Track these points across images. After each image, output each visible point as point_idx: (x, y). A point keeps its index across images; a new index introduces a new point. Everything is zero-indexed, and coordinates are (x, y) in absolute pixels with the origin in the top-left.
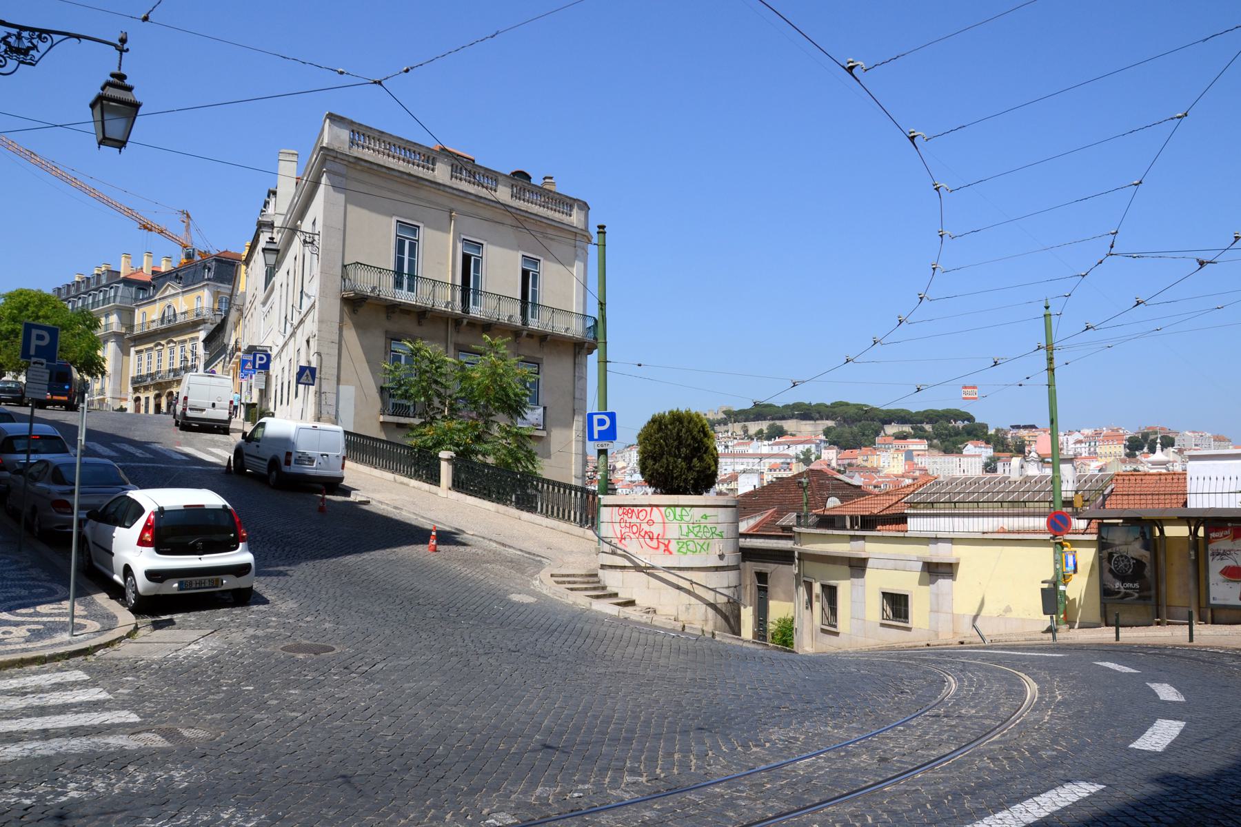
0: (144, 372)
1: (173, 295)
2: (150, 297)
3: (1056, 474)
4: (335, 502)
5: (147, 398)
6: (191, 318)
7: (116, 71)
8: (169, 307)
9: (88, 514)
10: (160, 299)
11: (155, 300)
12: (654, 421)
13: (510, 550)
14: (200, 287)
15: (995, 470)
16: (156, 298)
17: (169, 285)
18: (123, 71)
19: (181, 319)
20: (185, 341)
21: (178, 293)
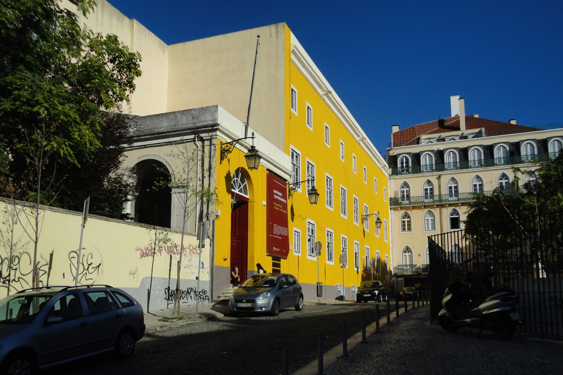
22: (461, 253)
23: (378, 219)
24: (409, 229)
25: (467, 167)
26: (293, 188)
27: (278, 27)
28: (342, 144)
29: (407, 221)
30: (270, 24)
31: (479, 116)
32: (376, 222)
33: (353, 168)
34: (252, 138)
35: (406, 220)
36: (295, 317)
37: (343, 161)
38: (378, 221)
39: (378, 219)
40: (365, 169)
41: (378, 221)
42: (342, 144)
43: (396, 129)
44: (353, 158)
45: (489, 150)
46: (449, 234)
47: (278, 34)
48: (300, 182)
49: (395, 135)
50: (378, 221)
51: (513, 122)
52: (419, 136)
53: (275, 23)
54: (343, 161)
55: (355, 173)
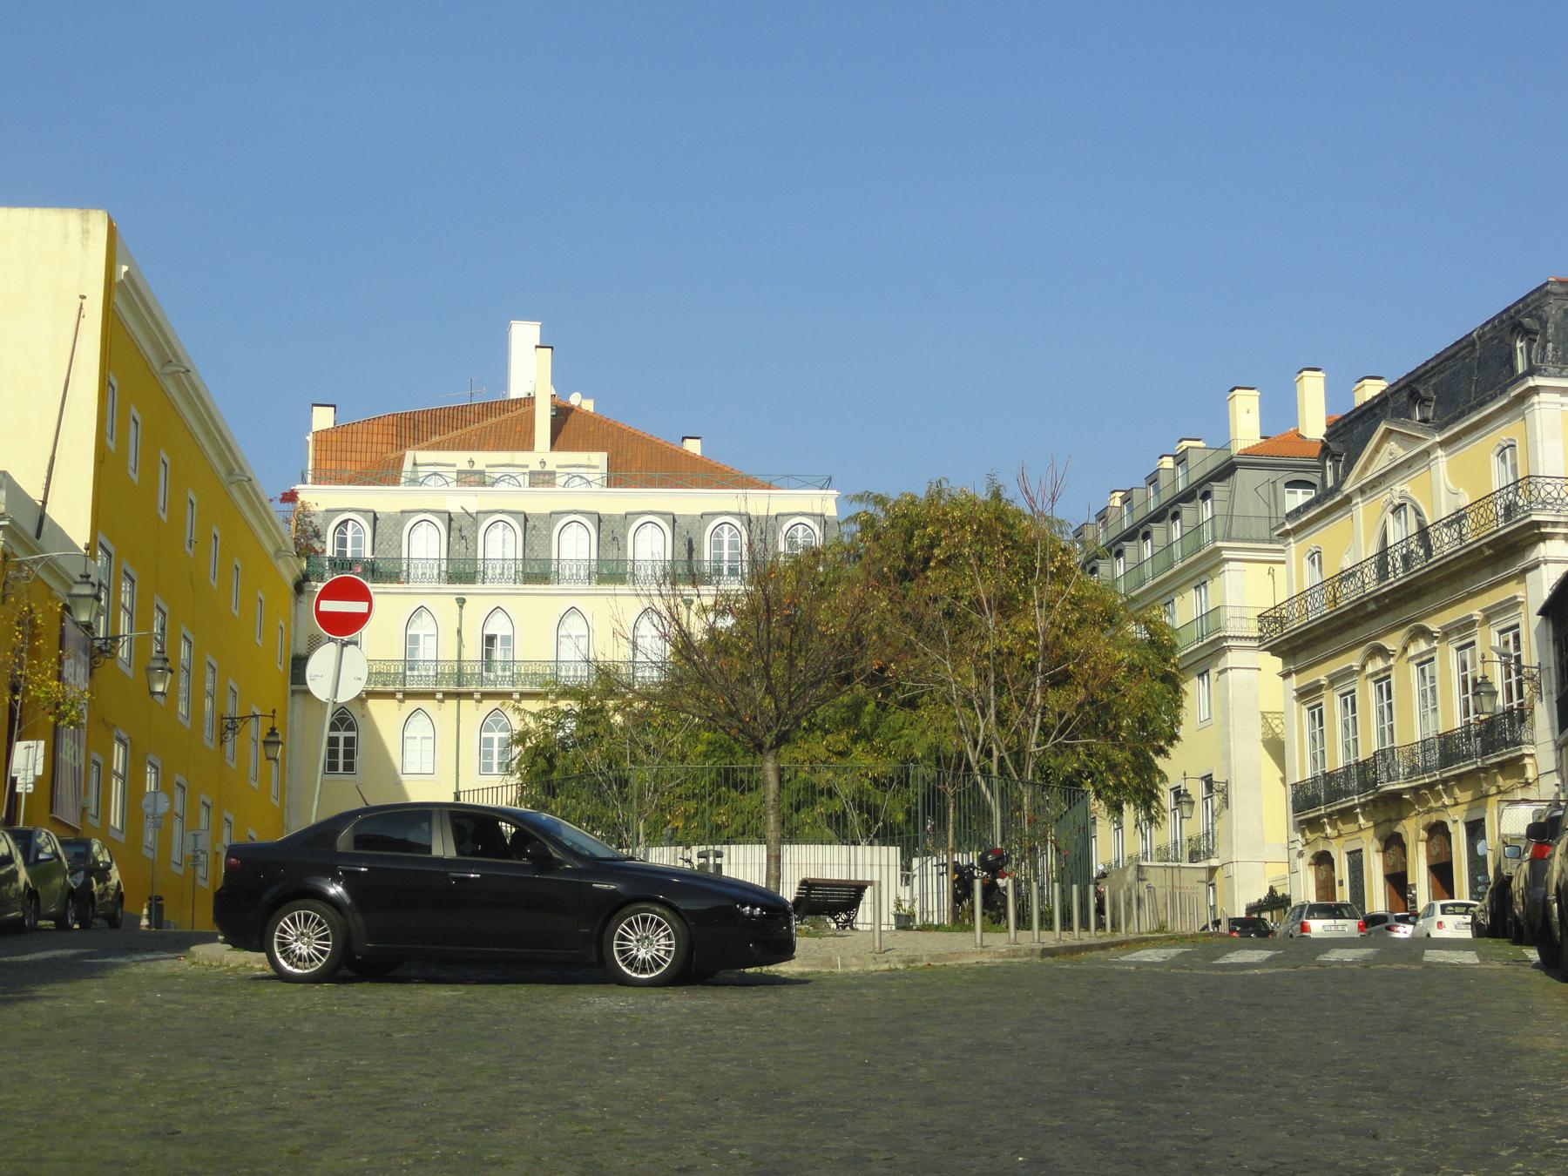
0: (1338, 760)
1: (1408, 464)
2: (1328, 494)
3: (612, 554)
4: (749, 974)
5: (1356, 859)
6: (1485, 527)
7: (82, 573)
8: (1397, 509)
9: (785, 950)
10: (1362, 491)
11: (1348, 500)
12: (1173, 738)
13: (163, 472)
14: (1503, 409)
15: (1094, 570)
16: (1348, 488)
17: (1389, 433)
18: (89, 572)
19: (1445, 544)
20: (1467, 625)
21: (1426, 453)
22: (112, 773)
23: (273, 732)
24: (349, 767)
25: (546, 578)
26: (104, 648)
27: (88, 220)
28: (136, 423)
29: (345, 738)
30: (66, 207)
31: (595, 406)
32: (266, 743)
33: (132, 464)
34: (273, 717)
35: (342, 735)
36: (94, 977)
37: (190, 552)
38: (272, 739)
39: (273, 732)
40: (216, 538)
41: (271, 739)
42: (136, 423)
43: (323, 419)
44: (133, 424)
45: (609, 531)
46: (490, 790)
47: (87, 239)
48: (124, 636)
49: (322, 436)
50: (271, 739)
51: (693, 447)
52: (400, 453)
53: (81, 208)
54: (190, 552)
55: (135, 477)
